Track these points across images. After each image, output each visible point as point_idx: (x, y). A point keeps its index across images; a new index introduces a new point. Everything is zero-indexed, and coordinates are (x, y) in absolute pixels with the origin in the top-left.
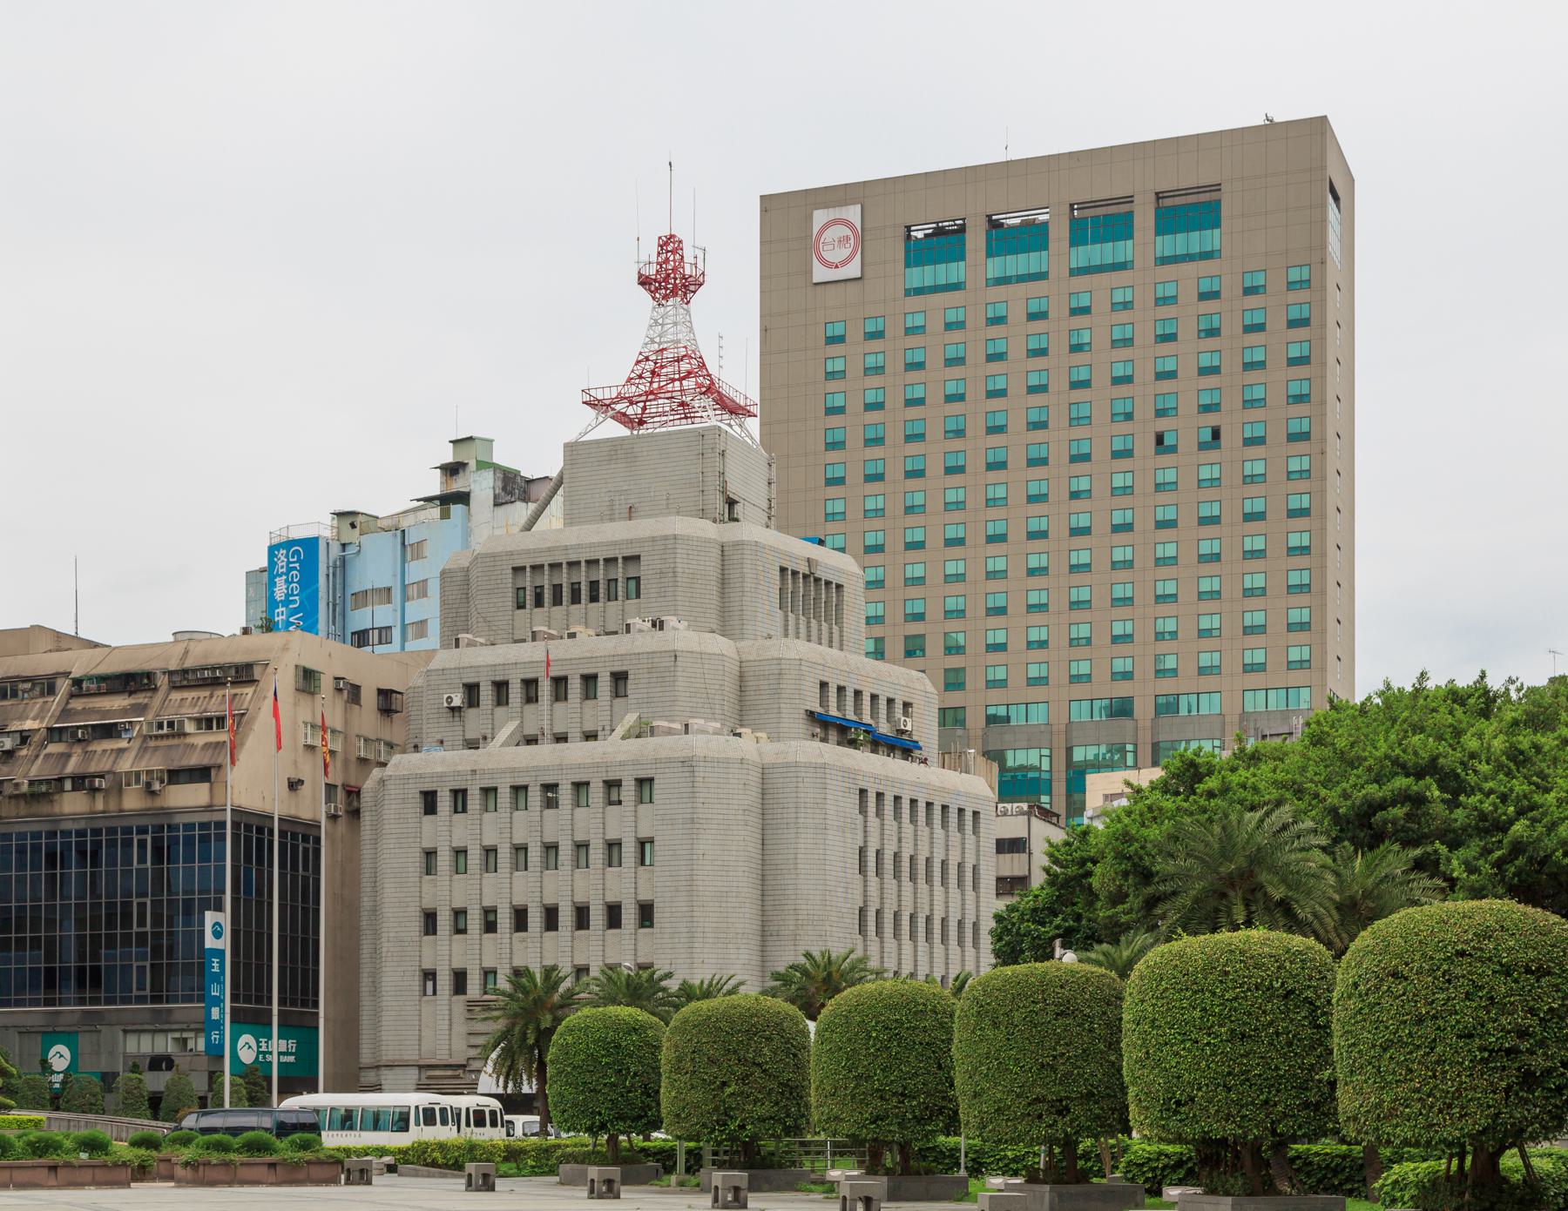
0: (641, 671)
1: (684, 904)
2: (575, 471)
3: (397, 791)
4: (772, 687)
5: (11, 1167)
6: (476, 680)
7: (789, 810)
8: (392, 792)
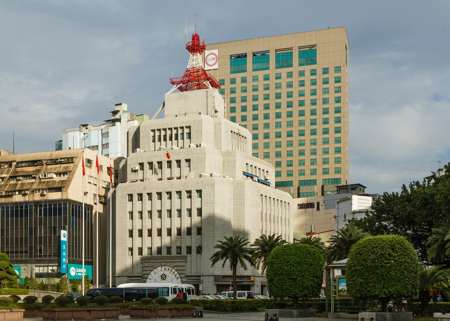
0: (195, 159)
1: (212, 228)
2: (168, 102)
3: (120, 194)
4: (233, 164)
5: (72, 311)
6: (143, 162)
7: (242, 200)
8: (119, 194)
